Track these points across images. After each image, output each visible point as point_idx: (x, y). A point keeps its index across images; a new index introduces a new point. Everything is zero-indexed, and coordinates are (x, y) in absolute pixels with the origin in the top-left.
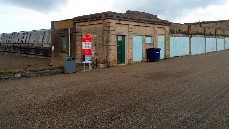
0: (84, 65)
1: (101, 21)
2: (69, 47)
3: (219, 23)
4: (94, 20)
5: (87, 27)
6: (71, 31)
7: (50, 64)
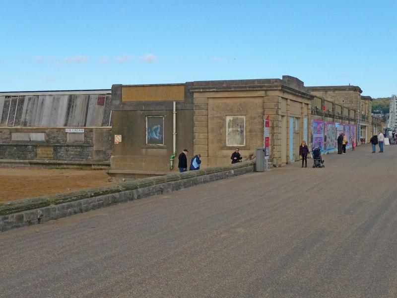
0: (267, 160)
1: (262, 93)
2: (174, 136)
3: (331, 92)
4: (246, 91)
5: (218, 101)
6: (179, 106)
7: (111, 171)
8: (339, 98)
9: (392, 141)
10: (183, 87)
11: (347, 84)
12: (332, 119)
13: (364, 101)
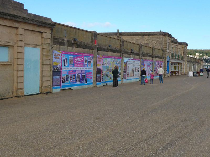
3: (147, 36)
8: (152, 42)
9: (195, 74)
10: (90, 34)
11: (158, 30)
12: (119, 54)
13: (181, 45)
